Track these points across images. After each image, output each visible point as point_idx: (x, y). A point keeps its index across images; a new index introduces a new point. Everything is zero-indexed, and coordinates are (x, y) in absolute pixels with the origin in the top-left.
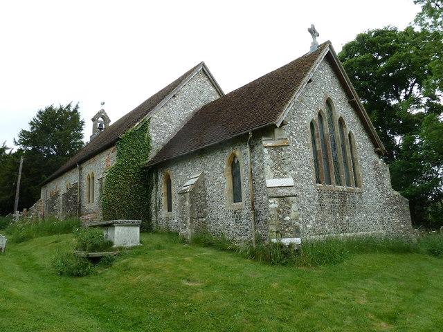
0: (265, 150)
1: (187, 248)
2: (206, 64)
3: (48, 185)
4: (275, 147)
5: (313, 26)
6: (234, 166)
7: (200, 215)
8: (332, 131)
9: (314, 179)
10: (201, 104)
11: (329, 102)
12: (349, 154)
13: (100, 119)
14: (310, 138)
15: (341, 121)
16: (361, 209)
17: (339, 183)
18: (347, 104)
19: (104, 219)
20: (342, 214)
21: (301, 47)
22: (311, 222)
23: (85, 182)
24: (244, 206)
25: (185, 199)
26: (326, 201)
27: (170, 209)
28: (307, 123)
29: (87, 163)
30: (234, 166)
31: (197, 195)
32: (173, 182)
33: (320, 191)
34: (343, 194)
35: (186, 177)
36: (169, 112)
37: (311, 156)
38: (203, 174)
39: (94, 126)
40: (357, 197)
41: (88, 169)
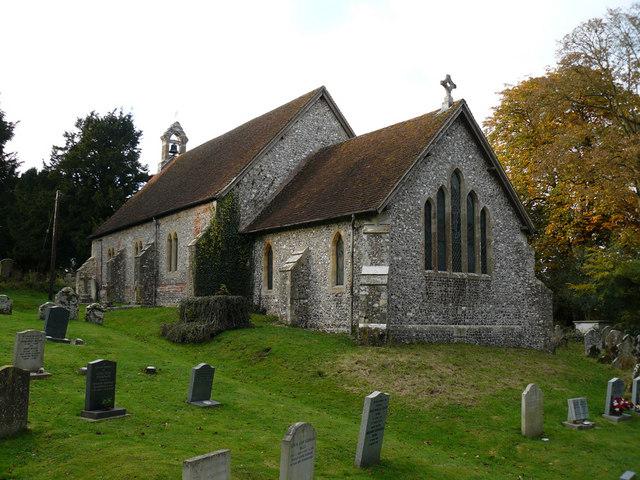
0: (365, 237)
1: (409, 368)
2: (328, 89)
3: (104, 239)
4: (375, 234)
5: (449, 77)
6: (338, 242)
7: (302, 296)
8: (456, 208)
9: (423, 265)
10: (318, 146)
11: (457, 173)
12: (478, 235)
13: (174, 137)
14: (422, 220)
15: (472, 195)
16: (487, 299)
17: (457, 268)
18: (485, 173)
19: (197, 295)
20: (458, 304)
21: (431, 101)
22: (413, 310)
23: (164, 244)
24: (345, 287)
25: (285, 278)
26: (436, 290)
27: (270, 287)
28: (421, 203)
29: (167, 218)
30: (338, 242)
31: (301, 274)
32: (275, 255)
33: (428, 279)
34: (461, 283)
35: (288, 251)
36: (275, 160)
37: (422, 240)
38: (308, 251)
39: (166, 151)
40: (483, 285)
41: (168, 226)
